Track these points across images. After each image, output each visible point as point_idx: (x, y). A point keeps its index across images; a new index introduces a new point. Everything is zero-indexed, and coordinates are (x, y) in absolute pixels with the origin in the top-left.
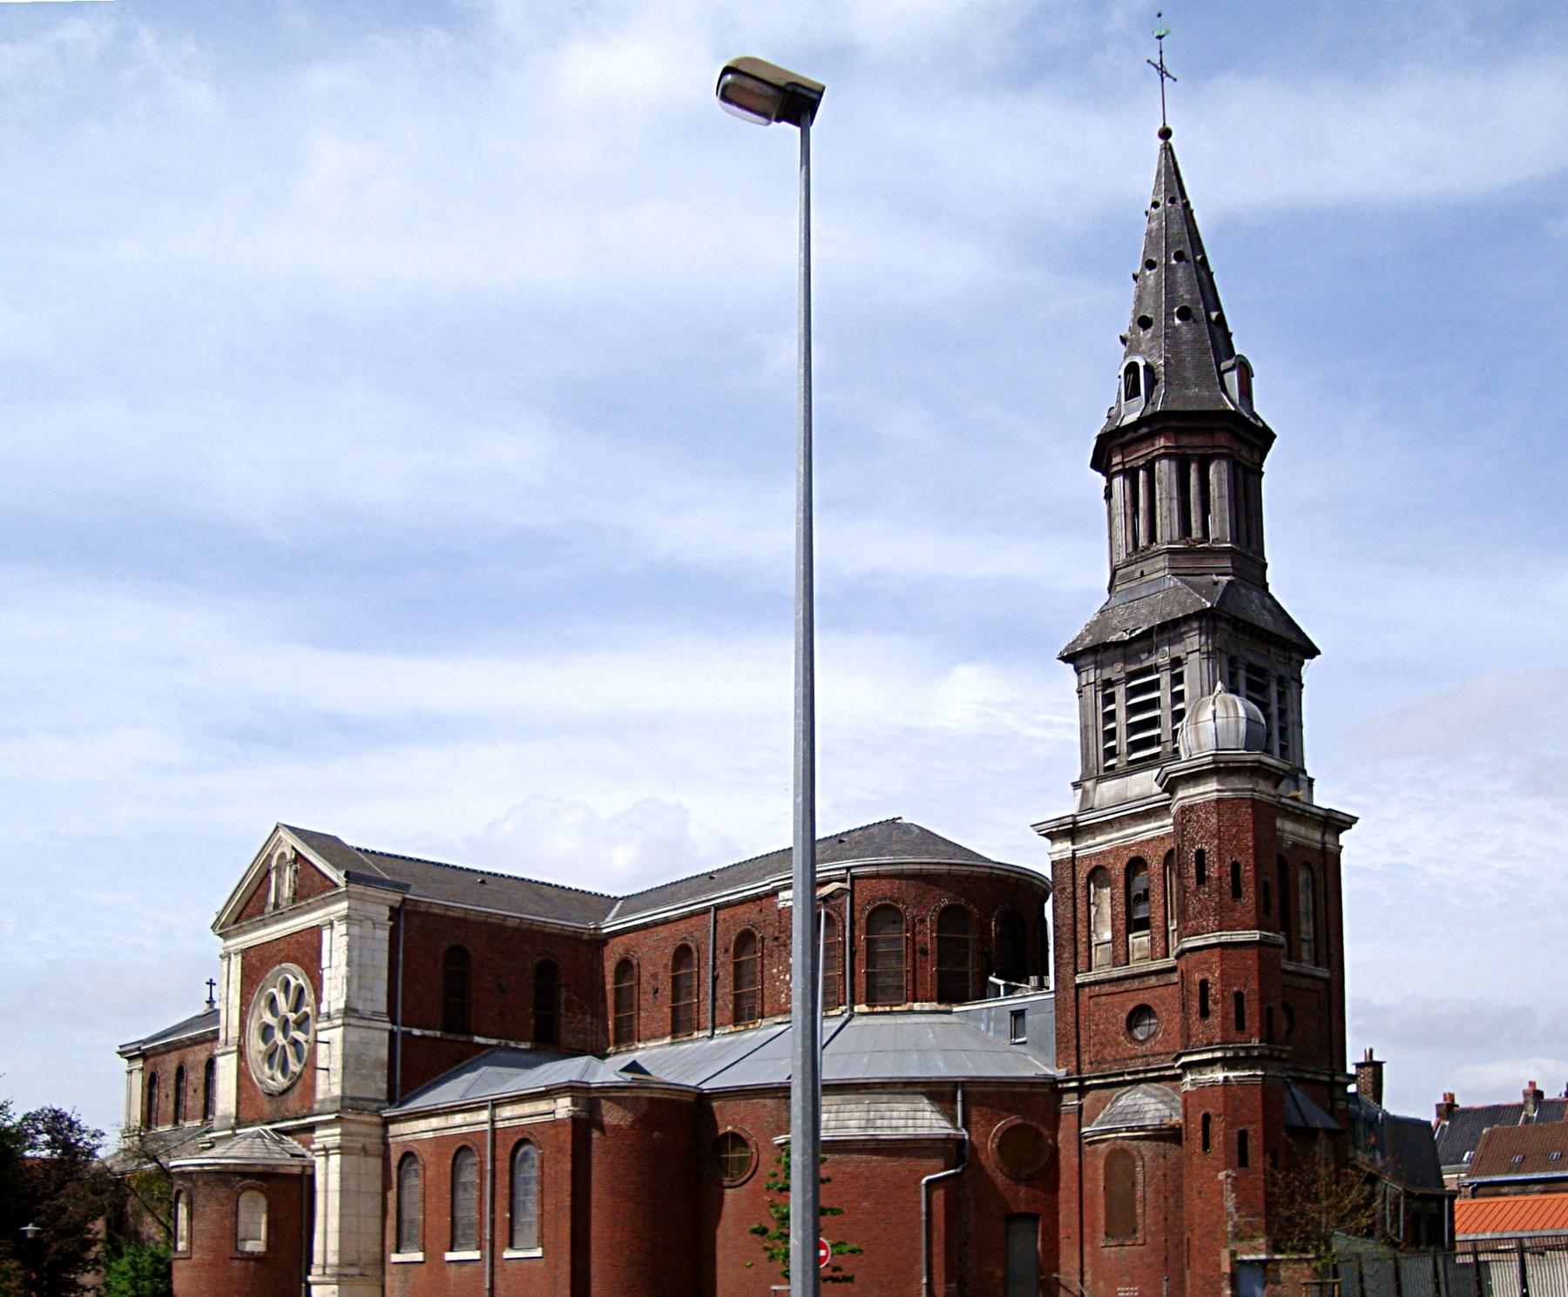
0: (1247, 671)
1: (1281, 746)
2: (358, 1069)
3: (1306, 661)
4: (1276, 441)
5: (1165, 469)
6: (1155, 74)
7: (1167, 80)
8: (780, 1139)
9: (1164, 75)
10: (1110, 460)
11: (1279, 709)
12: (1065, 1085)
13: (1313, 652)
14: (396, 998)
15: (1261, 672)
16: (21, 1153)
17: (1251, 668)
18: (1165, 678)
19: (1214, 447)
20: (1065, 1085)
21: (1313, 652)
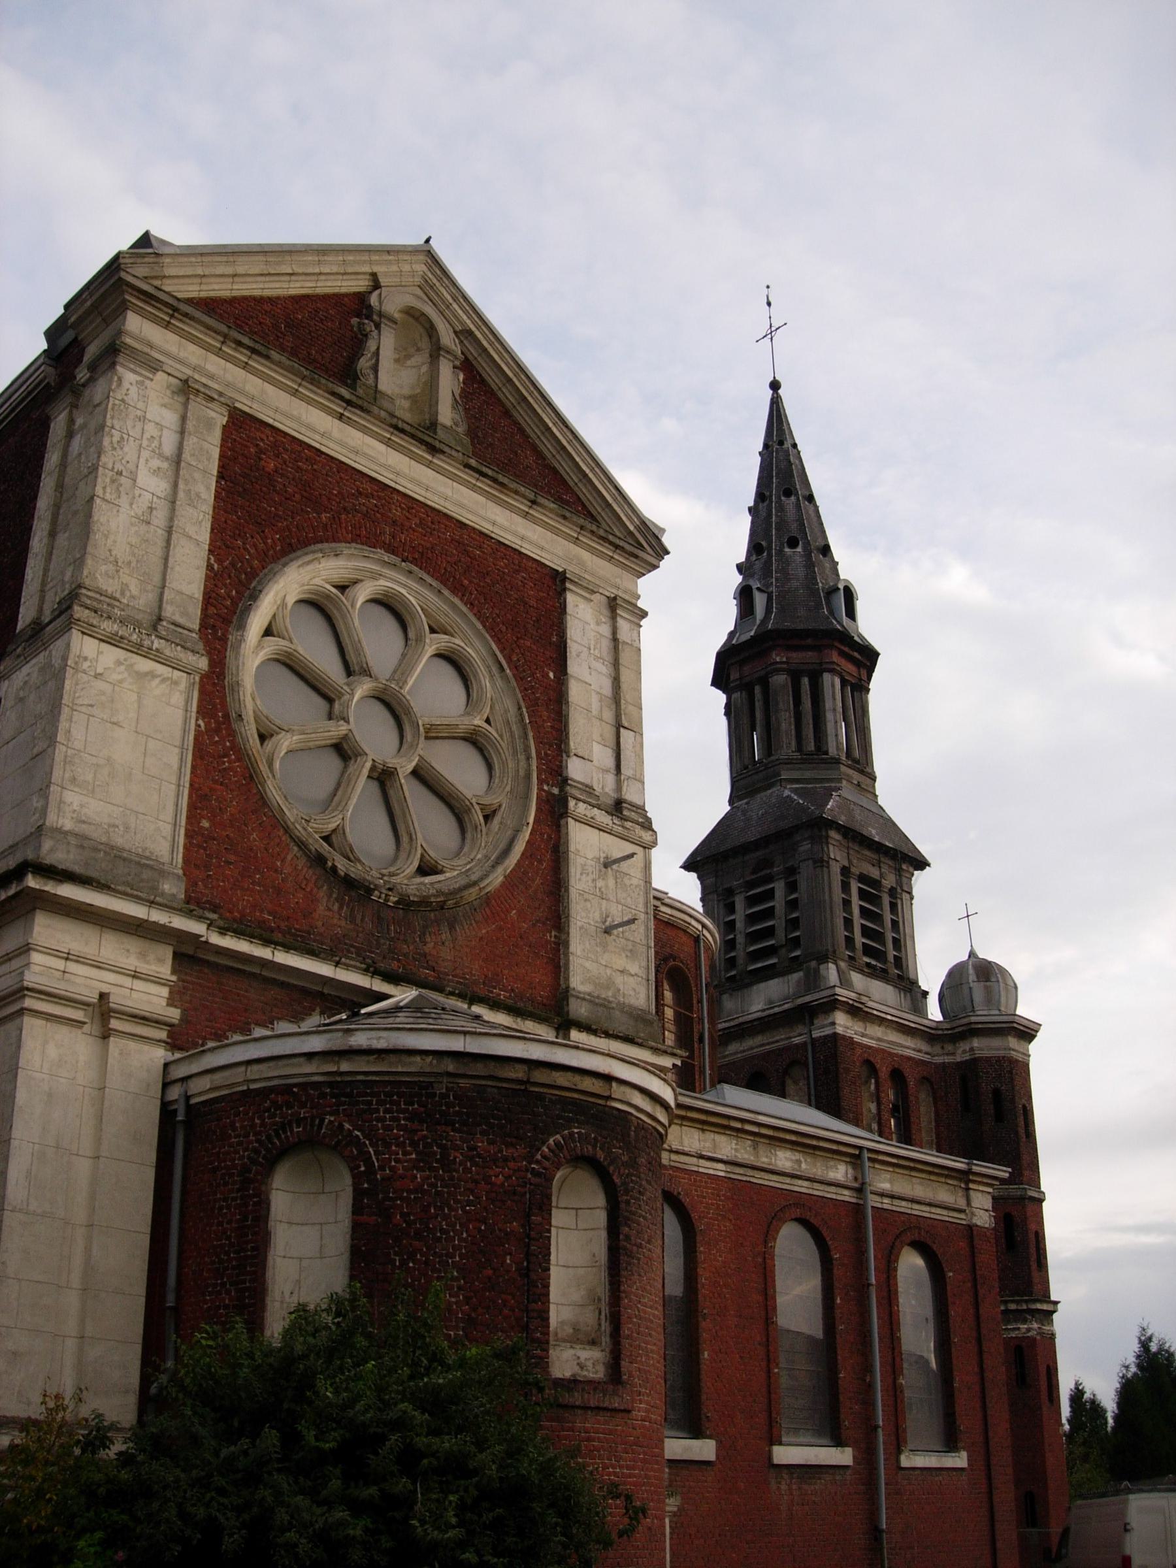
0: (861, 898)
1: (891, 903)
2: (508, 1356)
3: (916, 873)
4: (880, 657)
5: (780, 680)
6: (765, 329)
7: (775, 325)
8: (333, 1328)
9: (773, 329)
10: (728, 676)
11: (890, 902)
12: (50, 887)
13: (921, 864)
14: (171, 1174)
15: (875, 884)
16: (270, 1352)
17: (863, 878)
18: (779, 887)
19: (863, 1035)
20: (50, 887)
21: (921, 864)
